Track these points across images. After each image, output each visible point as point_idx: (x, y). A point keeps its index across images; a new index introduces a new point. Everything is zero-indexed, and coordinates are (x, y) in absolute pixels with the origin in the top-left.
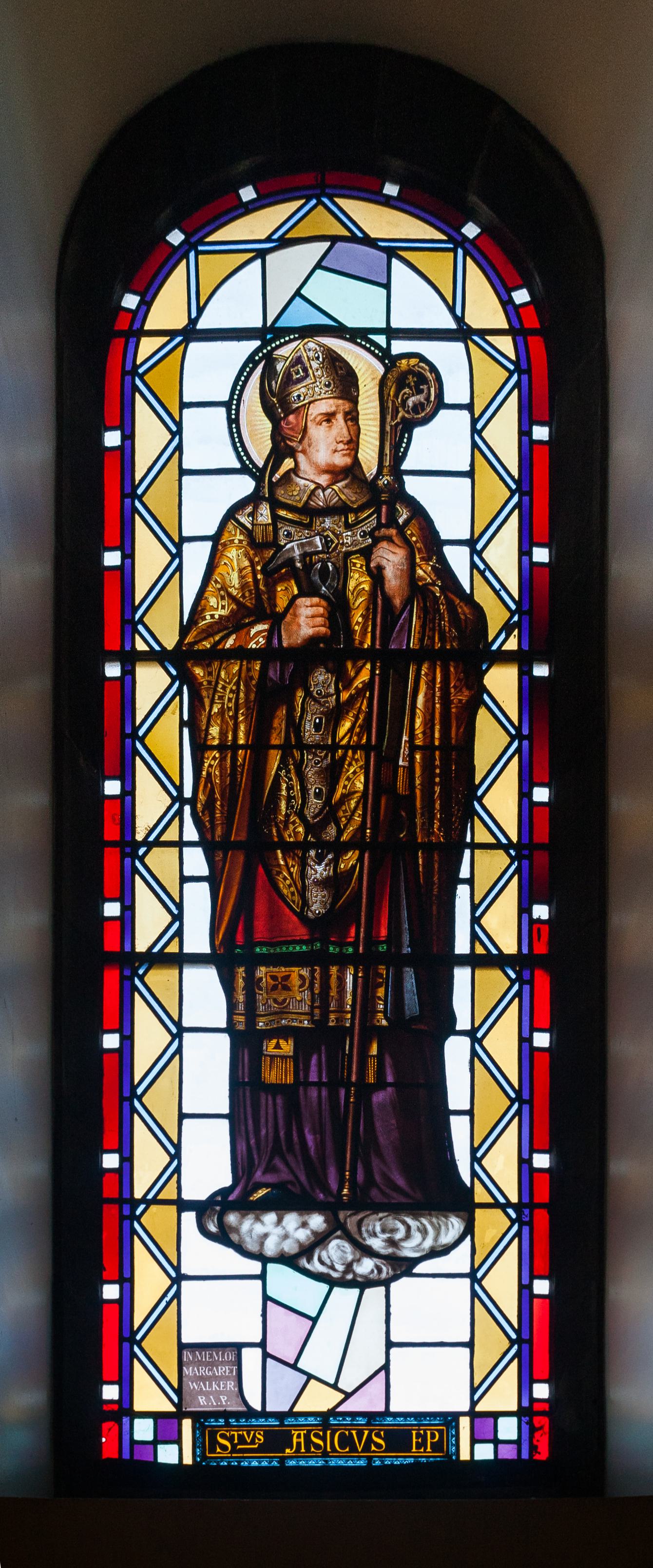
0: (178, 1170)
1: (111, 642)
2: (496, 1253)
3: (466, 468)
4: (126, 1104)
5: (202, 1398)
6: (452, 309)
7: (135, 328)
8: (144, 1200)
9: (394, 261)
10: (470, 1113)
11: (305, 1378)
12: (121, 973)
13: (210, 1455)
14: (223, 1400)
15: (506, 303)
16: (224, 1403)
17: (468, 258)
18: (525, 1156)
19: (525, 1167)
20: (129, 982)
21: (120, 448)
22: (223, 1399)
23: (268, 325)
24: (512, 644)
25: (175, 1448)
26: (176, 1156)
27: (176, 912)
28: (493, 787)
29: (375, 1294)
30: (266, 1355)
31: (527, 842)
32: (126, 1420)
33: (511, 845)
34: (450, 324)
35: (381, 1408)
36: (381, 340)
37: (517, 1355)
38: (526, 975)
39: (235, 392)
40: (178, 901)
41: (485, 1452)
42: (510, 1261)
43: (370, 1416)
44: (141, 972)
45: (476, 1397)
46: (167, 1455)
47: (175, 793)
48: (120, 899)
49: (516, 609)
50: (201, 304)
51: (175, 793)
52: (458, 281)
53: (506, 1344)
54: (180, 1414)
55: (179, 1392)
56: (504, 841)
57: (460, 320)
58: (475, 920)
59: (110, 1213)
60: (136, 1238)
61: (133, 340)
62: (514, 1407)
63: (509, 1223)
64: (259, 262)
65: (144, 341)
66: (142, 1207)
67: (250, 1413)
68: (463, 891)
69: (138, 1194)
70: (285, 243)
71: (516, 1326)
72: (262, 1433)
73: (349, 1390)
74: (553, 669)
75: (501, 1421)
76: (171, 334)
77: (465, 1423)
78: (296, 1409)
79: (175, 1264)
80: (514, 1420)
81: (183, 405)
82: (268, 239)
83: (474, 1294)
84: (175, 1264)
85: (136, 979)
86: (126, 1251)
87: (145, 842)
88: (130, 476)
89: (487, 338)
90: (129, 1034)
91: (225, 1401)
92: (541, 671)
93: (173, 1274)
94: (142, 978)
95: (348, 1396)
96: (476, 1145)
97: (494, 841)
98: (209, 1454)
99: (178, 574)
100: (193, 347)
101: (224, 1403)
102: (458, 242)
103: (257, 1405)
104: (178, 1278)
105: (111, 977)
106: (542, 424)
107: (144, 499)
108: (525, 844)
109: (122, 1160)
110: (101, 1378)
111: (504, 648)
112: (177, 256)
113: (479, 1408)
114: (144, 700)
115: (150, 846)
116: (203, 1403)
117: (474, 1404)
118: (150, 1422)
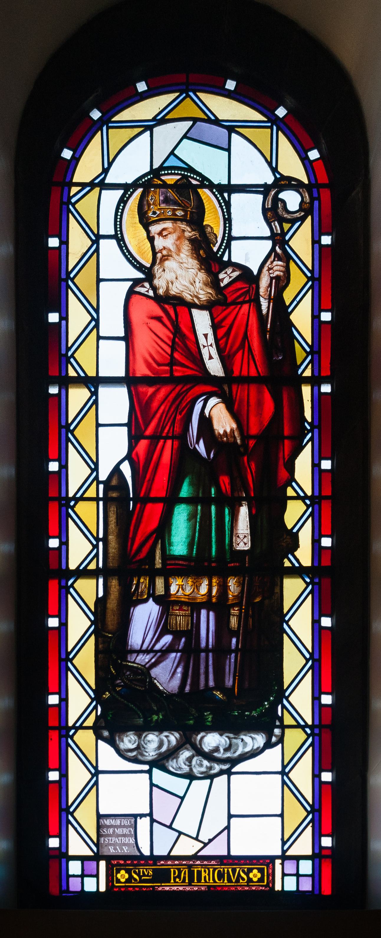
0: (96, 402)
1: (53, 372)
8: (74, 727)
9: (233, 135)
11: (177, 834)
12: (60, 583)
14: (125, 849)
18: (316, 462)
19: (316, 469)
24: (308, 373)
30: (153, 821)
32: (64, 861)
33: (306, 497)
35: (225, 853)
38: (317, 580)
41: (290, 885)
45: (286, 848)
46: (90, 885)
48: (59, 616)
49: (310, 810)
54: (97, 857)
55: (97, 845)
59: (54, 735)
62: (309, 852)
64: (148, 133)
67: (142, 856)
69: (70, 724)
72: (152, 870)
78: (172, 854)
79: (95, 765)
80: (309, 863)
82: (154, 119)
83: (284, 783)
87: (74, 498)
91: (126, 850)
95: (205, 845)
96: (285, 763)
98: (116, 883)
99: (94, 406)
102: (273, 120)
103: (146, 852)
104: (96, 773)
105: (53, 586)
108: (316, 318)
109: (61, 776)
110: (47, 533)
112: (94, 129)
115: (77, 500)
117: (284, 852)
118: (78, 863)
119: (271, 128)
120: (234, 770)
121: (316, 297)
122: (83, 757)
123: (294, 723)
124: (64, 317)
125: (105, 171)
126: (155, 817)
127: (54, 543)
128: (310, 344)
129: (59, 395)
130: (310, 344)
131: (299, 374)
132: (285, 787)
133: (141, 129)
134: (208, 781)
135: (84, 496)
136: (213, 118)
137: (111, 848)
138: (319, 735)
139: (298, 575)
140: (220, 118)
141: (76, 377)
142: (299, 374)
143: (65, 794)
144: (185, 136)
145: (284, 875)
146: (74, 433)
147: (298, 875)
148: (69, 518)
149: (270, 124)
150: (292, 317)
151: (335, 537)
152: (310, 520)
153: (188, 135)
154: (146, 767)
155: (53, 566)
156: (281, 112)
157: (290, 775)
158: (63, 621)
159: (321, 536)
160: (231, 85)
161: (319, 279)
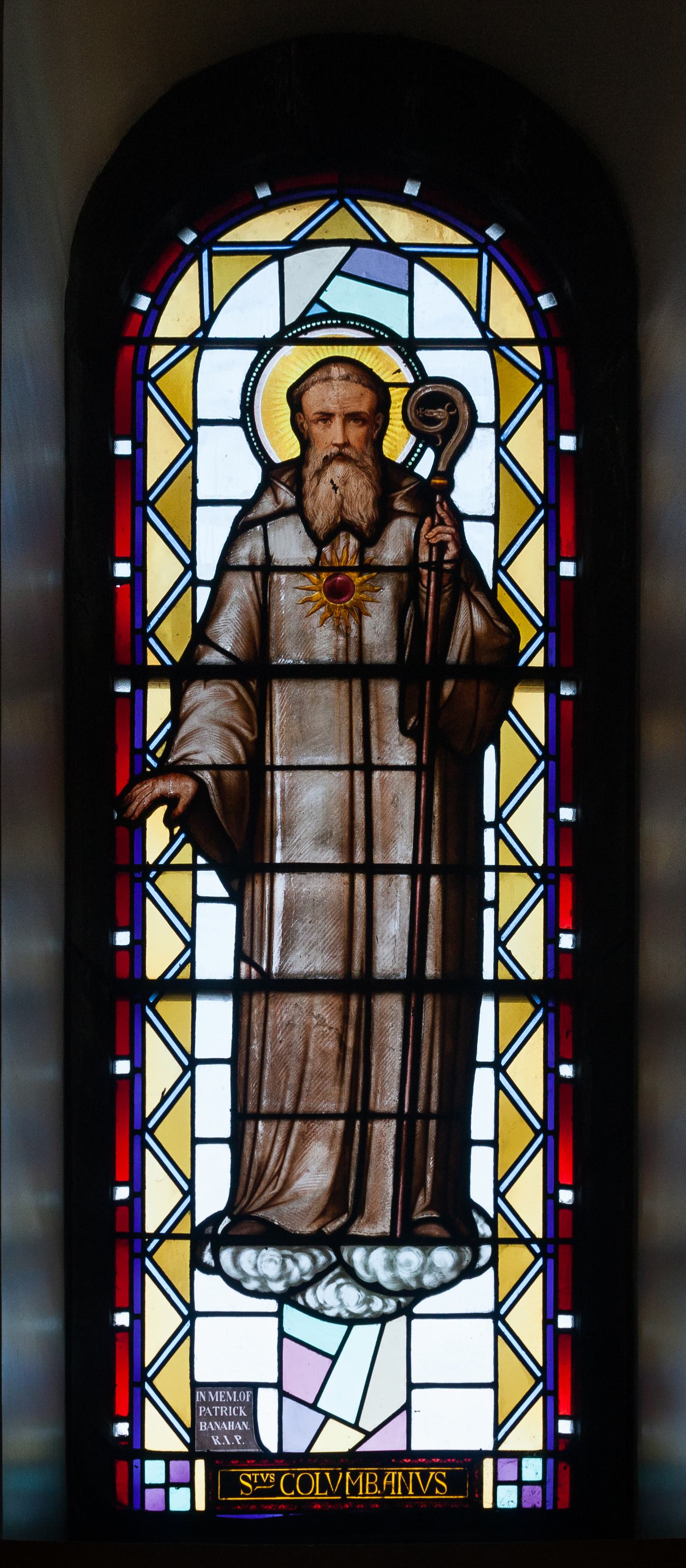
0: (193, 457)
2: (520, 1288)
4: (137, 1139)
5: (215, 1438)
6: (476, 316)
9: (417, 268)
10: (494, 1144)
15: (532, 309)
16: (239, 1443)
17: (493, 264)
22: (238, 1438)
24: (538, 661)
25: (186, 1491)
26: (190, 945)
27: (188, 561)
28: (525, 1294)
30: (283, 1394)
33: (535, 868)
34: (476, 334)
37: (543, 1145)
39: (252, 373)
40: (190, 549)
41: (508, 1498)
46: (179, 1500)
50: (215, 307)
53: (530, 1381)
55: (191, 1431)
56: (529, 864)
57: (484, 326)
58: (499, 943)
59: (122, 1255)
62: (538, 1445)
64: (275, 265)
66: (156, 1241)
68: (488, 914)
69: (151, 859)
70: (305, 245)
71: (541, 1363)
73: (370, 1429)
74: (581, 569)
75: (525, 1461)
80: (538, 1462)
81: (198, 422)
82: (287, 241)
83: (497, 1332)
86: (137, 1040)
88: (141, 607)
89: (515, 348)
90: (140, 565)
92: (567, 691)
93: (186, 1312)
95: (368, 1435)
97: (517, 864)
100: (207, 354)
101: (239, 1443)
102: (483, 245)
103: (273, 1448)
104: (191, 1315)
106: (568, 433)
111: (530, 665)
112: (188, 258)
113: (503, 1447)
117: (497, 1443)
118: (161, 1464)
119: (479, 257)
120: (417, 1310)
121: (551, 1164)
123: (516, 863)
125: (206, 326)
126: (285, 1388)
127: (122, 1193)
128: (540, 368)
131: (524, 978)
134: (377, 1327)
135: (172, 863)
136: (384, 240)
141: (158, 666)
142: (524, 978)
144: (338, 271)
145: (497, 1483)
147: (519, 1483)
148: (148, 523)
149: (476, 251)
152: (540, 1277)
153: (342, 269)
154: (271, 1305)
157: (508, 1319)
158: (138, 1064)
159: (560, 558)
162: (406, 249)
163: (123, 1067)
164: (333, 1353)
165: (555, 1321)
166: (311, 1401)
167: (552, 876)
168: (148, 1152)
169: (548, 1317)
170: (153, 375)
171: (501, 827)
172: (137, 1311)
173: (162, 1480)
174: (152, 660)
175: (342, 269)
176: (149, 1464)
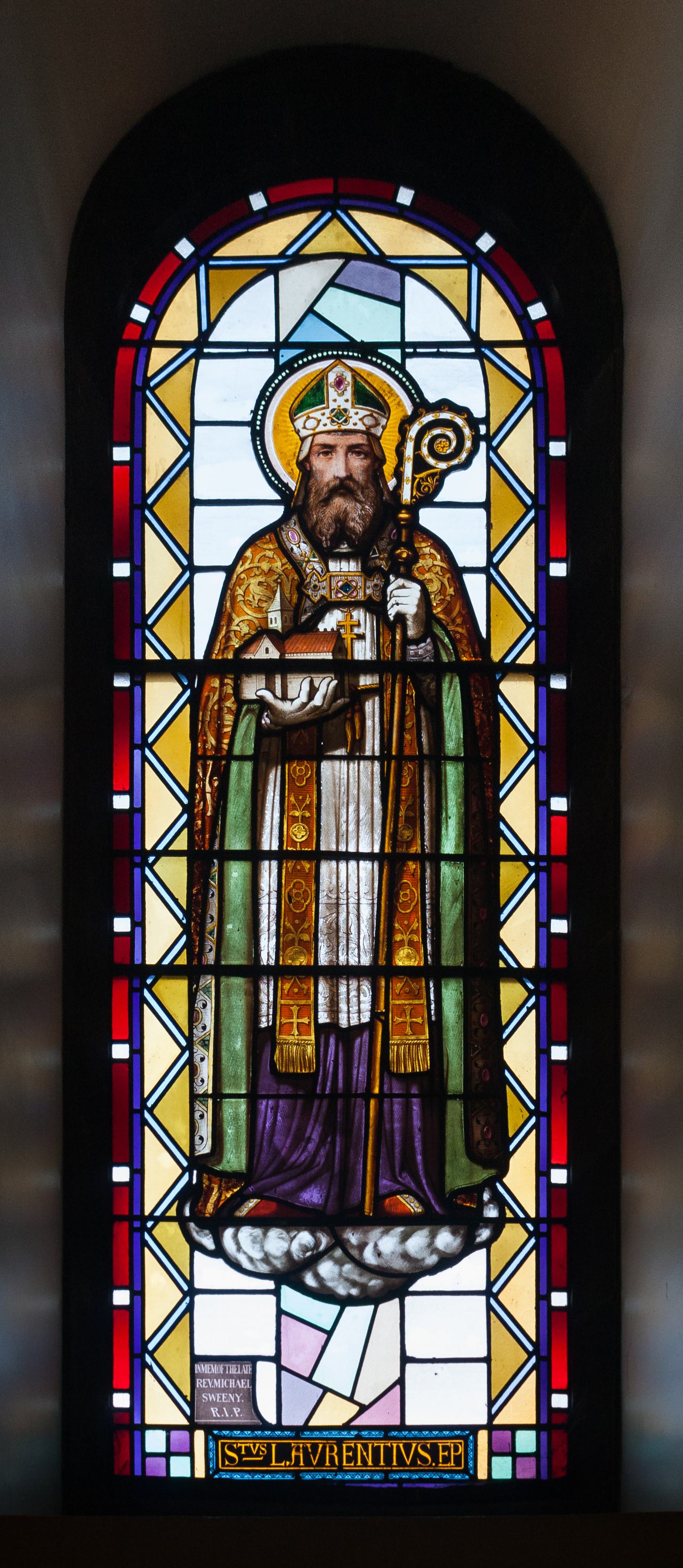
0: (190, 463)
3: (482, 499)
4: (138, 394)
6: (466, 325)
7: (145, 338)
9: (408, 280)
11: (321, 1391)
12: (131, 983)
13: (223, 1468)
14: (236, 1412)
15: (522, 319)
16: (237, 1415)
20: (139, 1115)
21: (130, 464)
23: (281, 340)
29: (389, 1309)
30: (280, 1368)
31: (545, 854)
35: (397, 1422)
36: (395, 354)
37: (536, 1126)
41: (502, 1469)
42: (528, 1272)
43: (386, 1429)
44: (149, 981)
45: (494, 1410)
46: (179, 1468)
47: (185, 562)
51: (185, 562)
52: (474, 298)
55: (191, 1404)
56: (522, 1215)
59: (121, 1230)
60: (145, 1006)
61: (143, 351)
63: (524, 627)
64: (271, 279)
65: (155, 351)
67: (266, 1426)
69: (149, 846)
70: (299, 259)
76: (184, 345)
77: (483, 1435)
80: (532, 1434)
81: (194, 423)
82: (282, 255)
83: (489, 1308)
84: (187, 552)
85: (147, 1356)
86: (137, 1264)
87: (154, 851)
91: (238, 1413)
92: (558, 683)
93: (186, 1288)
94: (150, 988)
95: (363, 1408)
101: (237, 1415)
103: (272, 1419)
104: (191, 1292)
105: (120, 990)
106: (557, 439)
107: (154, 748)
113: (497, 1421)
114: (153, 713)
115: (158, 855)
116: (215, 1415)
117: (491, 1417)
118: (162, 1434)
122: (168, 1263)
124: (139, 923)
126: (284, 1363)
128: (530, 377)
129: (130, 690)
130: (530, 377)
132: (493, 586)
133: (260, 271)
137: (215, 1410)
138: (548, 1234)
139: (514, 979)
140: (388, 253)
143: (139, 1387)
145: (491, 1454)
146: (153, 989)
150: (504, 810)
151: (571, 1167)
152: (533, 1255)
153: (336, 281)
155: (118, 958)
156: (486, 243)
159: (551, 1391)
160: (405, 196)
161: (548, 1115)
162: (393, 261)
163: (121, 570)
164: (328, 1328)
165: (548, 1299)
166: (307, 1375)
167: (543, 864)
168: (146, 1250)
169: (541, 1293)
170: (152, 384)
171: (492, 571)
172: (137, 1166)
173: (163, 1450)
174: (150, 655)
175: (336, 281)
176: (149, 1434)
